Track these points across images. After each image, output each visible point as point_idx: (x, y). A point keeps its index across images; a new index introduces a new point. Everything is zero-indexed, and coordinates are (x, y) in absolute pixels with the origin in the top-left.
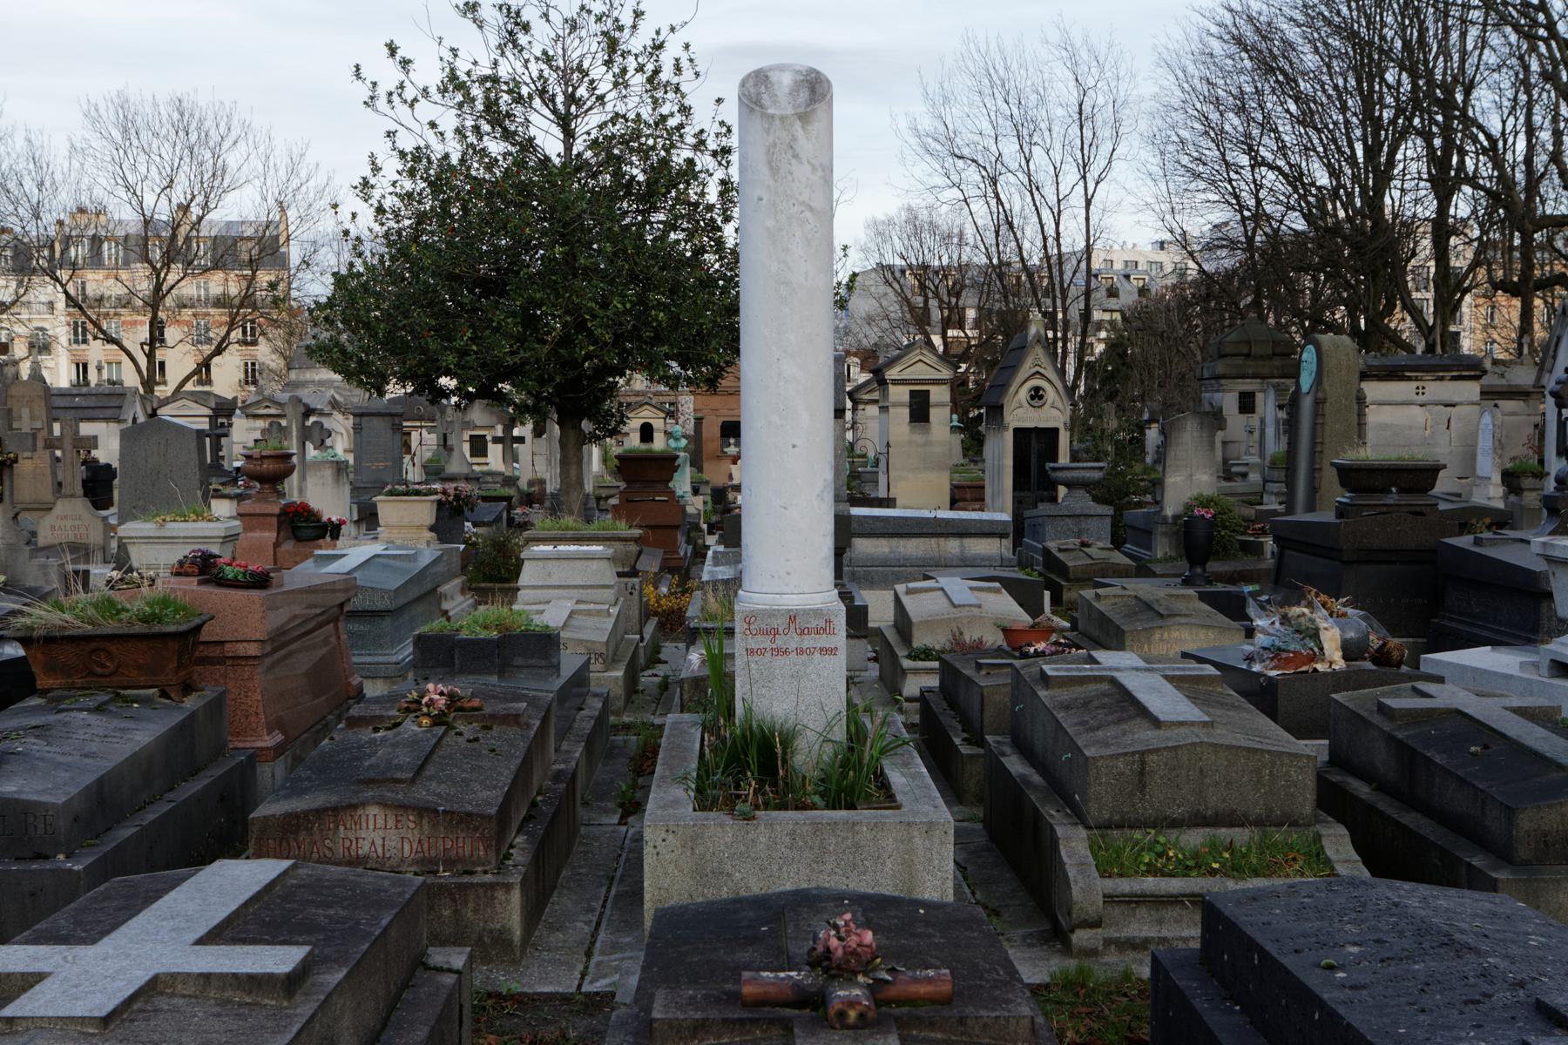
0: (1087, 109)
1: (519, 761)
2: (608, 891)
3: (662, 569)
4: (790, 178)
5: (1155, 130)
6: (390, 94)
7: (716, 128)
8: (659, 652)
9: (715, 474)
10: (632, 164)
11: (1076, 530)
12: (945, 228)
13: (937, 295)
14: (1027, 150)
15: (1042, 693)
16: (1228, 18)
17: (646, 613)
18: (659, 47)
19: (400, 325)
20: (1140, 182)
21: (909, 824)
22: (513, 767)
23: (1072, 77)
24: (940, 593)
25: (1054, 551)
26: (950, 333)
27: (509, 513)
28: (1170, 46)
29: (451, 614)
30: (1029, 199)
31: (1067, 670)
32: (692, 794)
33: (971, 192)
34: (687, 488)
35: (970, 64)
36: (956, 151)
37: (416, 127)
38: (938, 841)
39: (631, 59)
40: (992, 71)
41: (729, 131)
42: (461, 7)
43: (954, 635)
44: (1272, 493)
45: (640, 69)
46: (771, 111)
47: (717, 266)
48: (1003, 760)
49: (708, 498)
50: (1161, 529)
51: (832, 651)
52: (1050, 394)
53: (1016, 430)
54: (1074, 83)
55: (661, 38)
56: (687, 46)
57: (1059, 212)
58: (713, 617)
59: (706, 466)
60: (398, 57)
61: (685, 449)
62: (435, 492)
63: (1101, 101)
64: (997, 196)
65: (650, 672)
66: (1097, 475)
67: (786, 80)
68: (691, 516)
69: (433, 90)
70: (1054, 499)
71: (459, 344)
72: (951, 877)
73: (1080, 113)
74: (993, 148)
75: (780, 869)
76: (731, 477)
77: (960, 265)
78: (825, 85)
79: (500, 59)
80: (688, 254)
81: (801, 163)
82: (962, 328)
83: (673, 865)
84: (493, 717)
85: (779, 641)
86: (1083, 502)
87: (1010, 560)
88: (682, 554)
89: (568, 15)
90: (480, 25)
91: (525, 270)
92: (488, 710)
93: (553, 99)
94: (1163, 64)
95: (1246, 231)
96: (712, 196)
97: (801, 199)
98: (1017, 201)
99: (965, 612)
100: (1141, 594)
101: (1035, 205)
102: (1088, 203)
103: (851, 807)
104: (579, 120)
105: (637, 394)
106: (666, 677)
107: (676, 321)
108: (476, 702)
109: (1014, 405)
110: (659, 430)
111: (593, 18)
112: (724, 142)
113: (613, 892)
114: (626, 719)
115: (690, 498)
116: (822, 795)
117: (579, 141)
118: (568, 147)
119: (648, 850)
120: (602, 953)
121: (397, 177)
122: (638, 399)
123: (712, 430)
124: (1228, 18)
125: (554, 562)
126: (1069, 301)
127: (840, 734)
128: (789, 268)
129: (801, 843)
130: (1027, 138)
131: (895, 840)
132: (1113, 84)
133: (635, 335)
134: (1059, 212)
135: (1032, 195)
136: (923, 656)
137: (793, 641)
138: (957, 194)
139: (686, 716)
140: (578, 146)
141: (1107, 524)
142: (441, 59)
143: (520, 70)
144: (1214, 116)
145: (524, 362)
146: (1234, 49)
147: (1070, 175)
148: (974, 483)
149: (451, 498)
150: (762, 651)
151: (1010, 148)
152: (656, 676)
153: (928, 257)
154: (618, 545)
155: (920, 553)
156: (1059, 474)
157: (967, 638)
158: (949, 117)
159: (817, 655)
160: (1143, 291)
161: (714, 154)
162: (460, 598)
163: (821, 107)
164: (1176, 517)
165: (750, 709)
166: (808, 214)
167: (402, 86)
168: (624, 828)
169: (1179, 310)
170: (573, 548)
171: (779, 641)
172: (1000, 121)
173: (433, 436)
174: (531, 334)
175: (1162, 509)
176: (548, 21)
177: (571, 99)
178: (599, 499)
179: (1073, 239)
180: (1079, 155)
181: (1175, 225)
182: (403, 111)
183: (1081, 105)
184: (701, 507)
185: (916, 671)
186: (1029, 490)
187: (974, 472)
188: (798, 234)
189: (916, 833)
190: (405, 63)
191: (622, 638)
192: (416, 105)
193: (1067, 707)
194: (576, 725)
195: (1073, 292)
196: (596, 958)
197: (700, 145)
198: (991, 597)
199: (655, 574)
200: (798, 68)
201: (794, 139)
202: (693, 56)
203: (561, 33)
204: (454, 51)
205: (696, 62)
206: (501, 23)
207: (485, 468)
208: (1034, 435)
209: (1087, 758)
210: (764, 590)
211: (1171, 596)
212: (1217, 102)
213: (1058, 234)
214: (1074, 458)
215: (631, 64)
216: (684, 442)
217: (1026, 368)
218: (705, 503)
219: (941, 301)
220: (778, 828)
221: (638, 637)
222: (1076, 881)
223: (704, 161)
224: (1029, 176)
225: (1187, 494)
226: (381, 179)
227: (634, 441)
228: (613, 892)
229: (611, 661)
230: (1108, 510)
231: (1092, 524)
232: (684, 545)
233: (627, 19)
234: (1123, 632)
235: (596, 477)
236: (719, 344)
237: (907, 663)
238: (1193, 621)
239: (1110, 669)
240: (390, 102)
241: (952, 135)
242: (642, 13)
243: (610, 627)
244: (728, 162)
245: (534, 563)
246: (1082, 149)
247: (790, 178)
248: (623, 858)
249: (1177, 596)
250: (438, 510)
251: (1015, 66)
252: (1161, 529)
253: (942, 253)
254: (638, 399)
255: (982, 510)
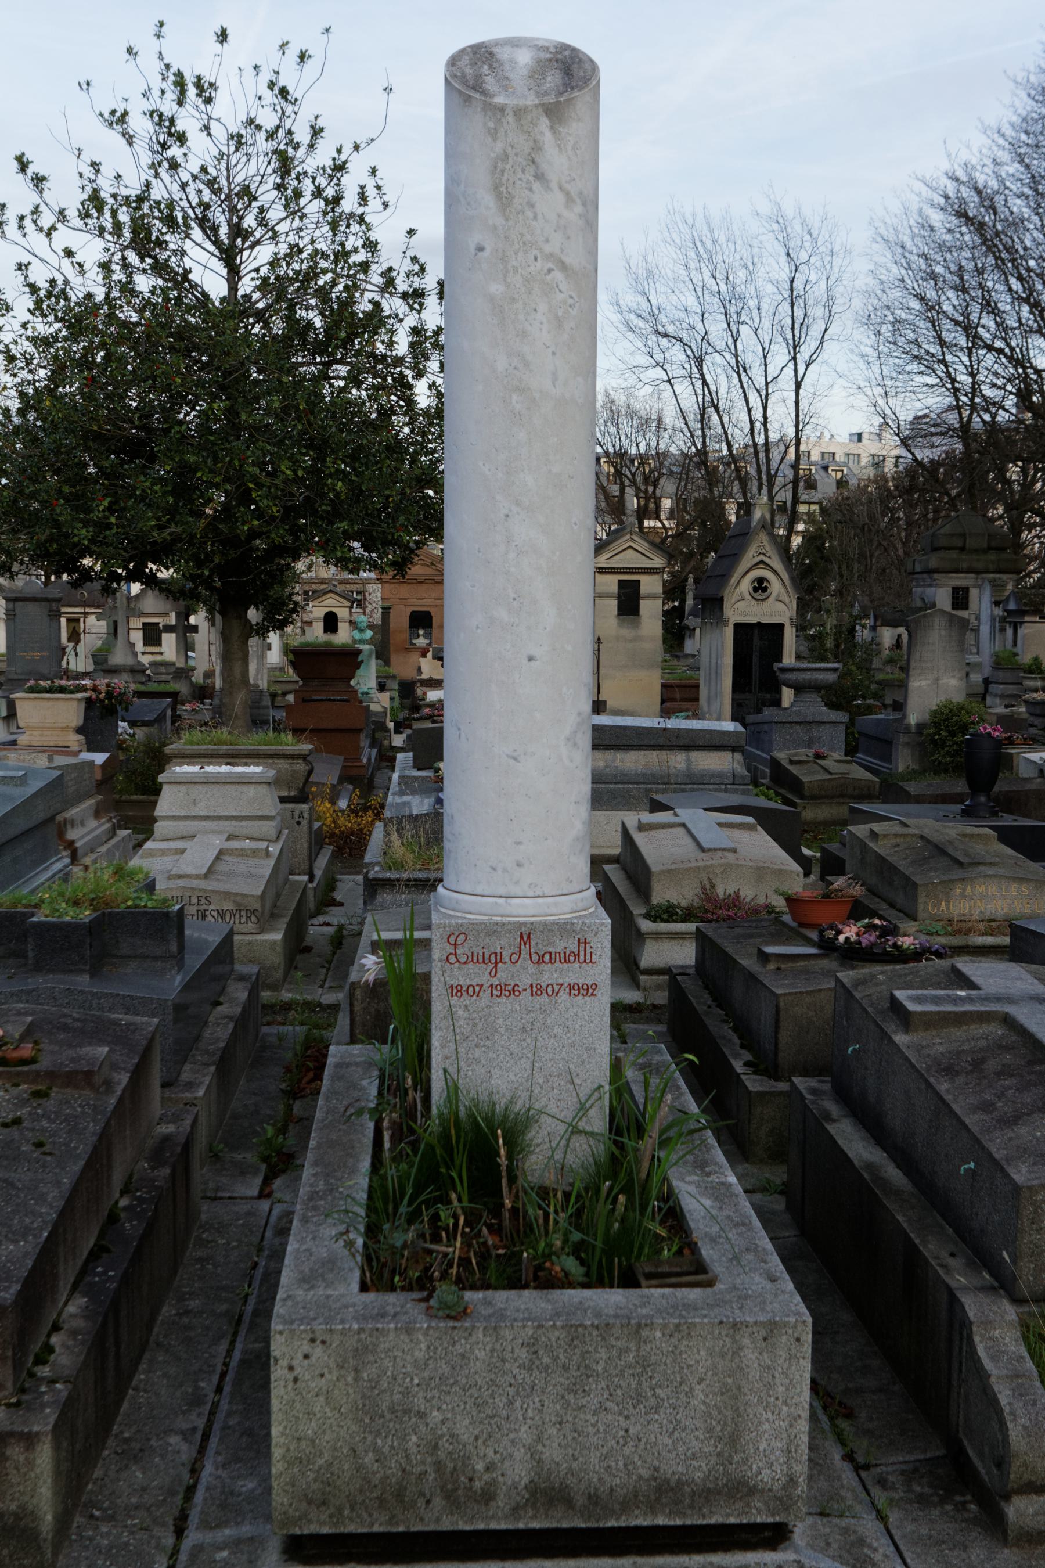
0: (798, 284)
1: (77, 1167)
2: (230, 1352)
3: (342, 779)
4: (529, 214)
5: (871, 308)
6: (22, 218)
7: (407, 266)
8: (333, 889)
9: (403, 667)
10: (308, 308)
11: (806, 738)
12: (643, 413)
13: (633, 483)
14: (734, 329)
15: (900, 1039)
16: (951, 188)
17: (318, 840)
18: (340, 168)
19: (27, 491)
20: (852, 365)
21: (735, 1325)
22: (67, 1182)
23: (783, 252)
24: (681, 831)
25: (785, 763)
26: (647, 523)
27: (174, 710)
28: (888, 220)
29: (78, 845)
30: (736, 380)
31: (936, 1000)
32: (359, 1258)
33: (675, 371)
34: (373, 683)
35: (675, 236)
36: (660, 329)
37: (53, 260)
38: (784, 1354)
39: (308, 182)
40: (699, 244)
41: (422, 269)
42: (107, 115)
43: (704, 888)
44: (996, 695)
45: (318, 193)
46: (499, 100)
47: (406, 430)
48: (828, 1127)
49: (396, 694)
50: (903, 738)
51: (588, 990)
52: (775, 586)
53: (737, 626)
54: (785, 258)
55: (343, 157)
56: (374, 171)
57: (767, 395)
58: (399, 865)
59: (394, 659)
60: (30, 171)
61: (371, 642)
62: (84, 689)
63: (813, 278)
64: (702, 375)
65: (321, 919)
66: (832, 677)
67: (524, 58)
68: (376, 714)
69: (72, 214)
70: (777, 703)
71: (94, 516)
72: (805, 1414)
73: (792, 290)
74: (699, 326)
75: (511, 1403)
76: (419, 670)
77: (658, 453)
78: (587, 66)
79: (154, 181)
80: (374, 416)
81: (548, 188)
82: (658, 517)
83: (322, 1399)
84: (52, 1076)
85: (504, 974)
86: (815, 707)
87: (743, 777)
88: (365, 761)
89: (234, 129)
90: (130, 140)
91: (177, 428)
92: (45, 1063)
93: (215, 229)
94: (879, 239)
95: (961, 418)
96: (402, 348)
97: (548, 249)
98: (725, 386)
99: (716, 860)
100: (926, 832)
101: (742, 387)
102: (798, 385)
103: (629, 1281)
104: (246, 254)
105: (323, 581)
106: (341, 927)
107: (357, 493)
108: (27, 1050)
109: (735, 597)
110: (344, 621)
111: (263, 135)
112: (417, 282)
113: (237, 1355)
114: (286, 995)
115: (375, 694)
116: (578, 1250)
117: (246, 280)
118: (233, 288)
119: (278, 1373)
120: (206, 1525)
121: (29, 317)
122: (323, 587)
123: (400, 620)
124: (951, 188)
125: (200, 787)
126: (776, 489)
127: (597, 1121)
128: (527, 364)
129: (546, 1360)
130: (735, 316)
131: (711, 1353)
132: (827, 259)
133: (309, 507)
134: (767, 395)
135: (739, 376)
136: (665, 916)
137: (525, 974)
138: (659, 373)
139: (356, 1049)
140: (246, 286)
141: (841, 732)
142: (81, 175)
143: (177, 195)
144: (931, 294)
145: (176, 539)
146: (955, 221)
147: (780, 356)
148: (684, 682)
149: (102, 696)
150: (475, 991)
151: (717, 329)
152: (328, 924)
153: (625, 442)
154: (283, 764)
155: (640, 768)
156: (789, 676)
157: (720, 892)
158: (653, 292)
159: (563, 996)
160: (841, 483)
161: (405, 296)
162: (93, 823)
163: (582, 98)
164: (921, 726)
165: (456, 1088)
166: (558, 275)
167: (36, 210)
168: (265, 1205)
169: (881, 502)
170: (225, 769)
171: (504, 974)
172: (707, 297)
173: (103, 623)
174: (185, 505)
175: (904, 716)
176: (209, 135)
177: (237, 231)
178: (273, 696)
179: (781, 424)
180: (789, 336)
181: (888, 412)
182: (38, 241)
183: (792, 282)
184: (387, 704)
185: (657, 936)
186: (750, 691)
187: (681, 670)
188: (542, 307)
189: (746, 1341)
190: (39, 181)
191: (287, 881)
192: (54, 234)
193: (949, 1071)
194: (207, 1034)
195: (779, 481)
196: (193, 1537)
197: (389, 283)
198: (745, 836)
199: (333, 786)
200: (540, 43)
201: (537, 147)
202: (380, 183)
203: (225, 150)
204: (95, 166)
205: (384, 189)
206: (152, 131)
207: (159, 658)
208: (756, 632)
209: (1016, 1189)
210: (479, 891)
211: (964, 835)
212: (933, 276)
213: (765, 417)
214: (798, 657)
215: (308, 187)
216: (369, 634)
217: (750, 557)
218: (392, 699)
219: (638, 489)
220: (508, 1334)
221: (305, 878)
222: (1012, 1413)
223: (392, 305)
224: (736, 356)
225: (934, 702)
226: (11, 320)
227: (317, 633)
228: (237, 1355)
229: (265, 919)
230: (843, 717)
231: (825, 732)
232: (367, 750)
233: (303, 136)
234: (915, 885)
235: (272, 669)
236: (409, 520)
237: (645, 925)
238: (1001, 871)
239: (998, 999)
240: (21, 227)
241: (656, 312)
242: (322, 130)
243: (267, 872)
244: (421, 305)
245: (172, 786)
246: (793, 329)
247: (529, 214)
248: (260, 1270)
249: (972, 836)
250: (86, 709)
251: (722, 239)
252: (903, 738)
253: (640, 439)
254: (323, 587)
255: (696, 716)
